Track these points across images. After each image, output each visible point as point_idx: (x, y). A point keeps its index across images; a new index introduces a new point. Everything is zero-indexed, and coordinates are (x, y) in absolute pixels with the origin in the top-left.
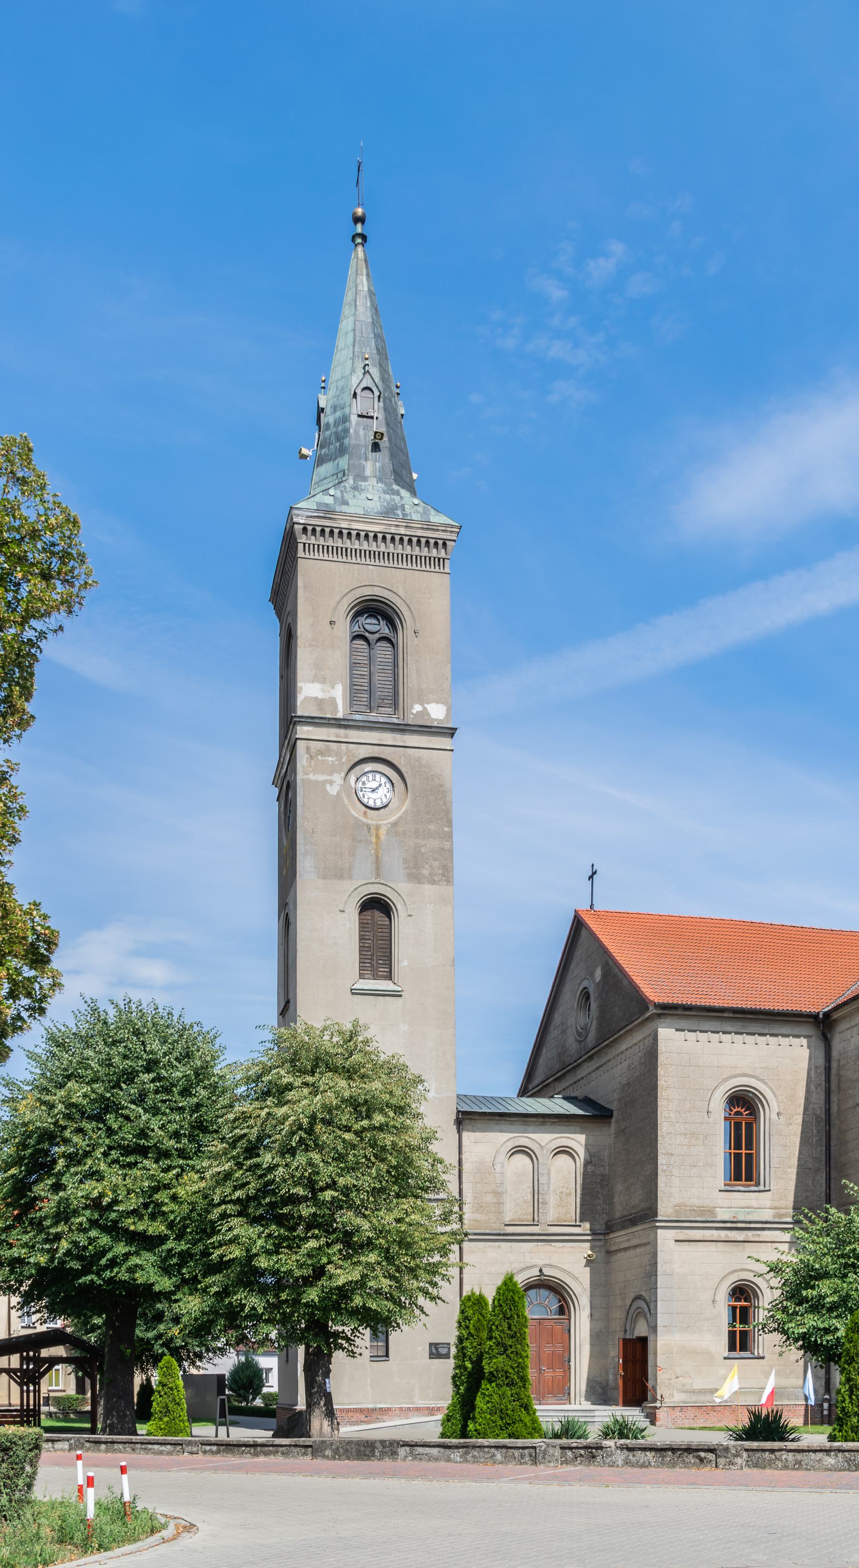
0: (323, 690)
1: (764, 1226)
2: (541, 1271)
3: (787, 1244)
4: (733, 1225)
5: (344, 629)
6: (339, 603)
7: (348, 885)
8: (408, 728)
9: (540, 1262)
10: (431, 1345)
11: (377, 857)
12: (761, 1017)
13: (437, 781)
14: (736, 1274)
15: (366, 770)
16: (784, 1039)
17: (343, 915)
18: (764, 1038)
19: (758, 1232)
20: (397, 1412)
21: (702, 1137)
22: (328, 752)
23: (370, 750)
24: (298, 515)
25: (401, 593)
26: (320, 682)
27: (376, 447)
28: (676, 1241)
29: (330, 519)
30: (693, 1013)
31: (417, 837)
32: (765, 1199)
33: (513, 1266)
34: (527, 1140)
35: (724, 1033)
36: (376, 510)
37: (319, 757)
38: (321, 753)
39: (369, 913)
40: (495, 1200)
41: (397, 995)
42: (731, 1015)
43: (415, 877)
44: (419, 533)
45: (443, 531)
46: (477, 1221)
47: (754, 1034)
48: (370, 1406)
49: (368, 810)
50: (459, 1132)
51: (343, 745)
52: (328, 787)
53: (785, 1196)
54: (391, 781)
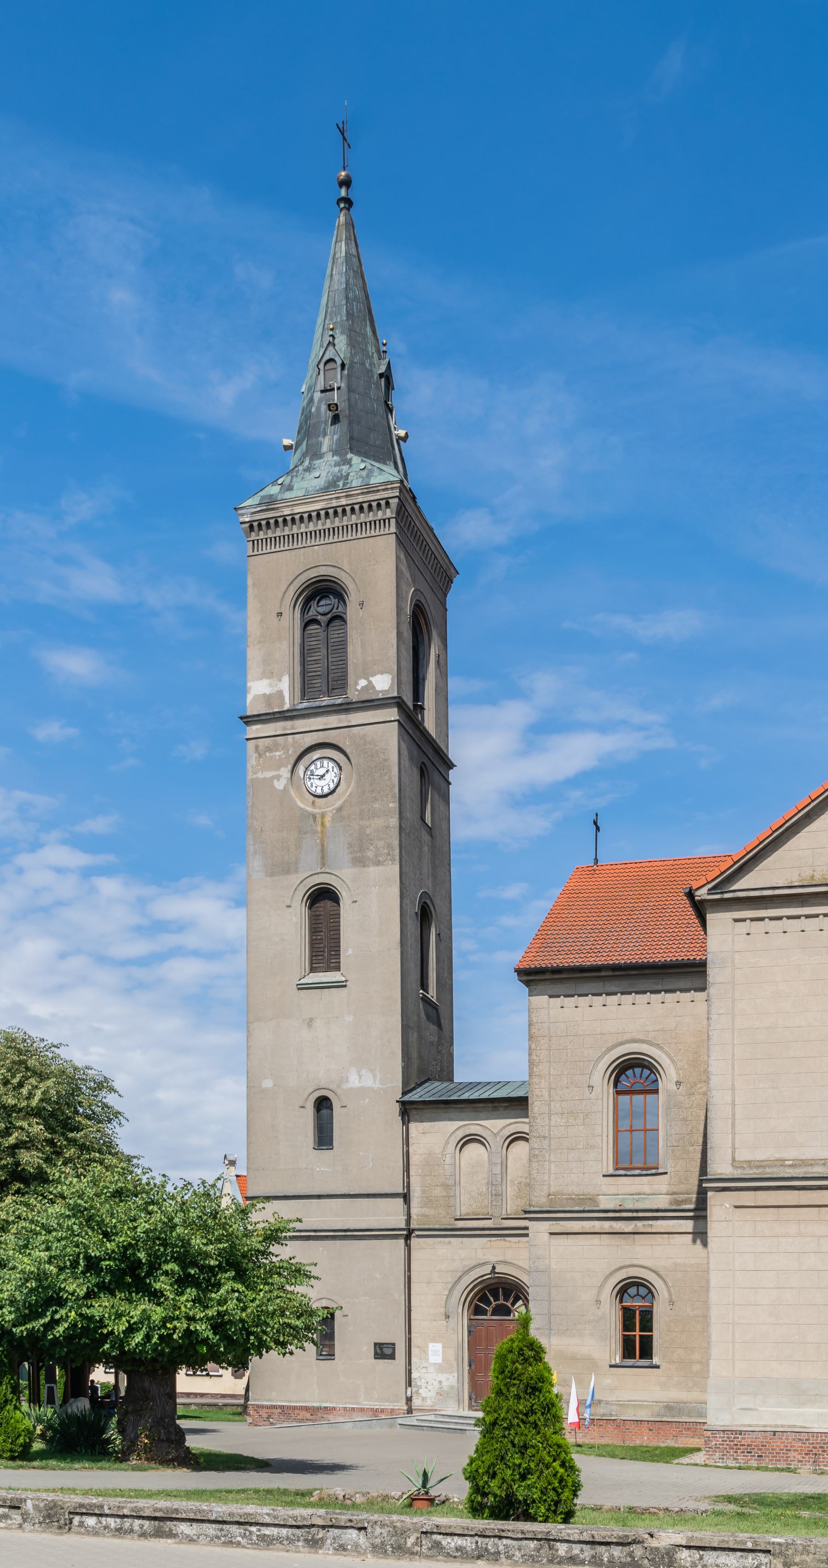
0: (271, 685)
1: (656, 1215)
2: (494, 1268)
3: (691, 1236)
5: (292, 620)
6: (285, 593)
8: (350, 706)
10: (376, 1344)
11: (323, 846)
12: (647, 972)
14: (624, 1270)
15: (314, 758)
16: (683, 994)
17: (290, 910)
19: (650, 1222)
20: (342, 1412)
21: (581, 1116)
22: (276, 747)
23: (316, 737)
24: (243, 515)
25: (346, 567)
26: (268, 678)
27: (336, 419)
28: (551, 1234)
29: (273, 509)
30: (564, 976)
31: (362, 819)
32: (661, 1184)
33: (465, 1263)
34: (478, 1127)
35: (608, 994)
36: (318, 488)
37: (267, 754)
38: (269, 749)
39: (321, 904)
40: (444, 1193)
41: (341, 985)
42: (611, 973)
43: (360, 861)
44: (361, 499)
45: (384, 490)
46: (426, 1216)
47: (644, 992)
48: (316, 1404)
49: (317, 800)
52: (276, 783)
53: (686, 1179)
54: (338, 764)
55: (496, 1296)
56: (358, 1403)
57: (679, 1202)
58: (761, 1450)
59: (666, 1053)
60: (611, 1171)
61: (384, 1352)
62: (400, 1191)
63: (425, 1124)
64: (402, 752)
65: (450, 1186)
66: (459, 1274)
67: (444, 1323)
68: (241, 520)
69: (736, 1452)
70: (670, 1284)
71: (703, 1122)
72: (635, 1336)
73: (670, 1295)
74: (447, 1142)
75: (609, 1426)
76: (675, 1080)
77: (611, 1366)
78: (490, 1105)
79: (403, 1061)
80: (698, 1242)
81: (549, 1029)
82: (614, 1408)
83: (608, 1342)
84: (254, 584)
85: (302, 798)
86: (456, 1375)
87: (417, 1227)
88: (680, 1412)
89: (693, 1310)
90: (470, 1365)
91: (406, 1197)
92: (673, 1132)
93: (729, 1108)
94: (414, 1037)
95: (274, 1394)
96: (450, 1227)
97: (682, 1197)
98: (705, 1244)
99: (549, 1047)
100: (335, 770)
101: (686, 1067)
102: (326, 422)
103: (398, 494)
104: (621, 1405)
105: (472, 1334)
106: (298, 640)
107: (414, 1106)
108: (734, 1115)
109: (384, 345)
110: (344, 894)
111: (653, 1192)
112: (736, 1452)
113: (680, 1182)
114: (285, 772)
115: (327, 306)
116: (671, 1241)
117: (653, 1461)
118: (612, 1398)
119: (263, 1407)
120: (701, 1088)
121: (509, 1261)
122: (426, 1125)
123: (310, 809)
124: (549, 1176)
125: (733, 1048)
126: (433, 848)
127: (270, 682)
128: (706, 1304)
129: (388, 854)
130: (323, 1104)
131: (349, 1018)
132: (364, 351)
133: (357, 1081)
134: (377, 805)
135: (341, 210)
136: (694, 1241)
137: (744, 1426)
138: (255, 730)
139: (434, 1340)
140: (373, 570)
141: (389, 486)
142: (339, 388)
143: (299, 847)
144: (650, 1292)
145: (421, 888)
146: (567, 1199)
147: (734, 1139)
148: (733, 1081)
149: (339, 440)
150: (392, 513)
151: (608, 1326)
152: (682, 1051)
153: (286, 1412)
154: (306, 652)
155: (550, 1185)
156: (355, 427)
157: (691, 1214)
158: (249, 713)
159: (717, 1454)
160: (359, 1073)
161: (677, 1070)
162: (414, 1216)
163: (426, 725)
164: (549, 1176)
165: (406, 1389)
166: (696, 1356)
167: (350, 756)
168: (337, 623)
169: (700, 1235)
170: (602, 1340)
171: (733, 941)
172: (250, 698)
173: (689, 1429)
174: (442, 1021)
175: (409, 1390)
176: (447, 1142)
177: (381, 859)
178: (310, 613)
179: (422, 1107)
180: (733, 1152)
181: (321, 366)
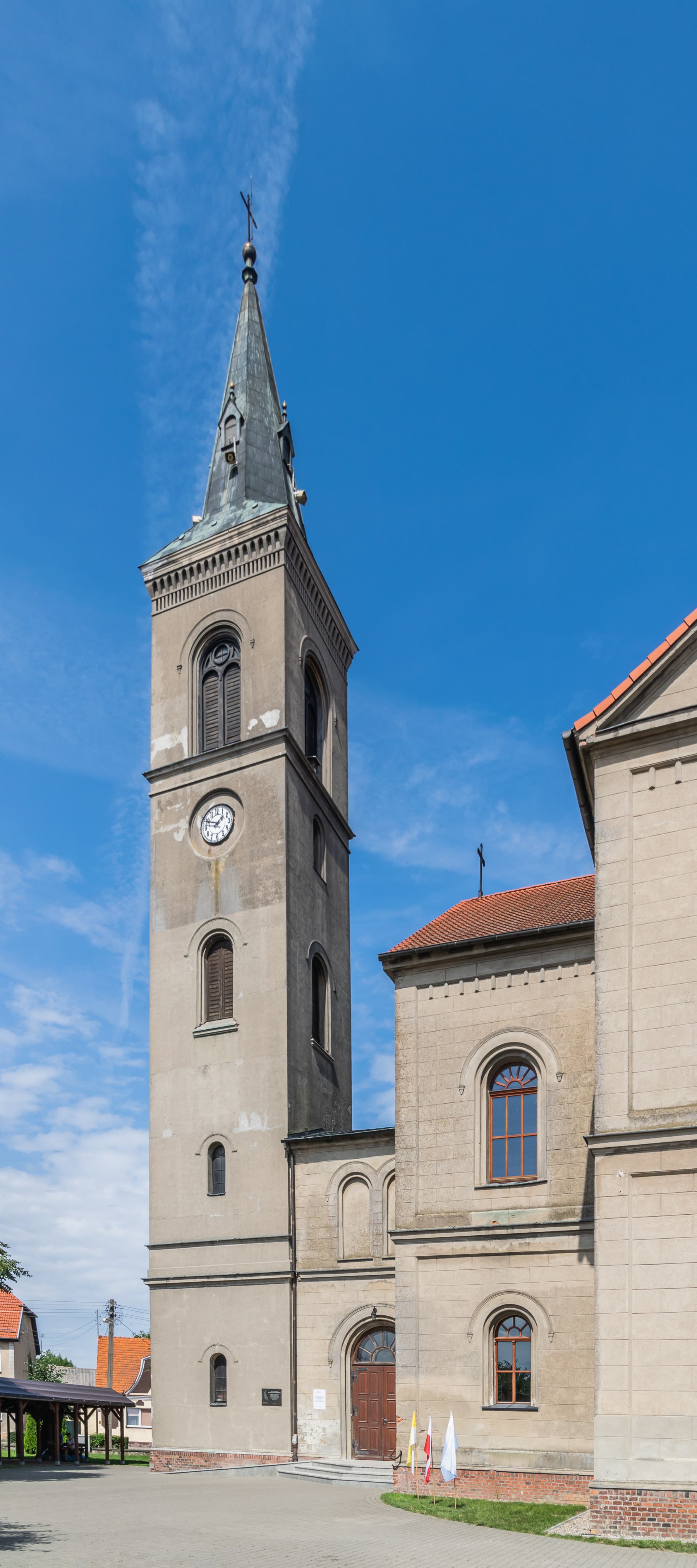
1: (533, 1230)
2: (375, 1310)
3: (576, 1255)
4: (489, 1233)
5: (191, 673)
7: (192, 928)
9: (374, 1301)
10: (263, 1390)
11: (217, 892)
12: (524, 944)
13: (271, 794)
14: (498, 1298)
17: (188, 959)
18: (537, 974)
19: (528, 1240)
21: (451, 1121)
22: (176, 800)
23: (211, 784)
24: (146, 573)
25: (239, 609)
26: (169, 733)
28: (419, 1258)
29: (173, 562)
31: (252, 860)
33: (347, 1306)
34: (360, 1165)
35: (481, 978)
37: (168, 808)
38: (170, 803)
40: (328, 1235)
41: (233, 1030)
42: (483, 951)
43: (250, 903)
44: (252, 534)
45: (273, 520)
47: (521, 971)
48: (209, 1451)
50: (291, 1165)
51: (188, 788)
53: (569, 1188)
55: (372, 1334)
56: (247, 1450)
57: (560, 1215)
58: (668, 1516)
59: (545, 1040)
60: (484, 1183)
61: (270, 1398)
62: (286, 1233)
63: (309, 1164)
64: (290, 790)
65: (335, 1227)
66: (342, 1318)
67: (328, 1368)
68: (146, 579)
69: (634, 1519)
70: (550, 1313)
71: (590, 1119)
72: (511, 1374)
73: (550, 1325)
74: (330, 1182)
75: (482, 1478)
76: (556, 1071)
77: (484, 1409)
78: (371, 1141)
79: (289, 1101)
80: (585, 1260)
81: (417, 1024)
82: (487, 1457)
83: (481, 1380)
84: (157, 642)
85: (199, 848)
86: (339, 1422)
87: (302, 1270)
88: (561, 1462)
89: (576, 1343)
90: (353, 1412)
91: (291, 1240)
92: (554, 1132)
93: (624, 1036)
94: (303, 1082)
95: (173, 1440)
96: (331, 1269)
97: (563, 1209)
98: (592, 1263)
99: (417, 1044)
100: (229, 816)
101: (568, 1055)
102: (226, 476)
103: (286, 522)
104: (494, 1454)
105: (355, 1380)
106: (196, 693)
107: (299, 1146)
108: (631, 1047)
109: (285, 408)
110: (235, 938)
111: (530, 1204)
112: (634, 1519)
113: (562, 1192)
114: (184, 824)
115: (230, 372)
116: (552, 1261)
117: (519, 1530)
118: (485, 1446)
119: (163, 1453)
120: (586, 1078)
121: (389, 1303)
122: (311, 1165)
123: (206, 858)
124: (417, 1193)
125: (631, 953)
126: (328, 905)
127: (170, 737)
128: (593, 1337)
129: (276, 893)
130: (216, 1151)
131: (240, 1063)
132: (264, 409)
133: (247, 1125)
134: (266, 845)
135: (246, 282)
136: (580, 1260)
137: (645, 1482)
138: (159, 785)
139: (319, 1387)
140: (261, 605)
141: (278, 515)
142: (237, 443)
143: (195, 896)
144: (528, 1323)
145: (314, 938)
146: (435, 1217)
147: (631, 1080)
148: (630, 997)
149: (236, 490)
150: (281, 544)
151: (481, 1362)
152: (564, 1036)
153: (183, 1457)
154: (205, 705)
155: (417, 1203)
156: (252, 478)
157: (577, 1228)
158: (152, 769)
159: (607, 1521)
160: (248, 1116)
161: (558, 1059)
162: (299, 1260)
163: (324, 783)
164: (417, 1193)
165: (292, 1436)
166: (580, 1397)
167: (242, 798)
168: (232, 671)
169: (587, 1252)
170: (471, 1379)
171: (631, 801)
172: (153, 754)
173: (571, 1483)
174: (338, 1077)
175: (295, 1436)
176: (330, 1182)
177: (269, 898)
178: (209, 666)
179: (306, 1147)
180: (630, 1099)
181: (222, 425)
